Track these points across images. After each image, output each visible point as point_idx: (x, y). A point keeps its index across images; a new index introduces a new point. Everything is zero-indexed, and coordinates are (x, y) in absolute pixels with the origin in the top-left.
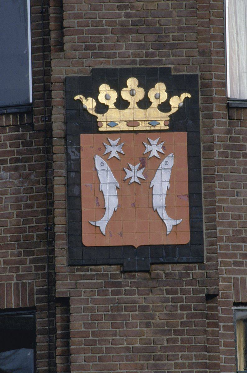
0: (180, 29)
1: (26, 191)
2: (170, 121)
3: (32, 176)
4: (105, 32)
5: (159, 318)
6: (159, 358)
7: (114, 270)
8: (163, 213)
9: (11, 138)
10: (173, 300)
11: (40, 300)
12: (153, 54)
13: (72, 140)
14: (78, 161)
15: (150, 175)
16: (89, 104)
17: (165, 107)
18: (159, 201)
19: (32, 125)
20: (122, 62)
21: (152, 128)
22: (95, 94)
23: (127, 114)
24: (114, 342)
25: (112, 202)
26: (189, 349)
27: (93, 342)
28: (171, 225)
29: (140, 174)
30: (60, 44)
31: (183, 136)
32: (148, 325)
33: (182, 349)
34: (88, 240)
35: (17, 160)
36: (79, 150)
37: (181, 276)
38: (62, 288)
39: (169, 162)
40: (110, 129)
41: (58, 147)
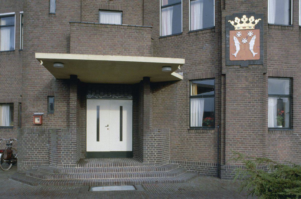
0: (258, 2)
1: (213, 48)
2: (255, 26)
4: (237, 4)
5: (250, 79)
6: (250, 90)
7: (238, 67)
8: (252, 51)
10: (254, 75)
11: (216, 76)
12: (250, 9)
13: (227, 33)
14: (229, 38)
15: (249, 41)
16: (232, 23)
17: (253, 23)
18: (251, 48)
19: (215, 31)
20: (241, 12)
21: (250, 29)
22: (234, 20)
23: (243, 25)
24: (238, 86)
25: (238, 48)
26: (258, 87)
27: (232, 86)
28: (255, 54)
29: (246, 41)
30: (224, 8)
31: (258, 30)
32: (247, 81)
33: (256, 87)
34: (231, 59)
35: (211, 41)
36: (229, 35)
37: (256, 68)
38: (224, 72)
39: (255, 37)
41: (223, 35)
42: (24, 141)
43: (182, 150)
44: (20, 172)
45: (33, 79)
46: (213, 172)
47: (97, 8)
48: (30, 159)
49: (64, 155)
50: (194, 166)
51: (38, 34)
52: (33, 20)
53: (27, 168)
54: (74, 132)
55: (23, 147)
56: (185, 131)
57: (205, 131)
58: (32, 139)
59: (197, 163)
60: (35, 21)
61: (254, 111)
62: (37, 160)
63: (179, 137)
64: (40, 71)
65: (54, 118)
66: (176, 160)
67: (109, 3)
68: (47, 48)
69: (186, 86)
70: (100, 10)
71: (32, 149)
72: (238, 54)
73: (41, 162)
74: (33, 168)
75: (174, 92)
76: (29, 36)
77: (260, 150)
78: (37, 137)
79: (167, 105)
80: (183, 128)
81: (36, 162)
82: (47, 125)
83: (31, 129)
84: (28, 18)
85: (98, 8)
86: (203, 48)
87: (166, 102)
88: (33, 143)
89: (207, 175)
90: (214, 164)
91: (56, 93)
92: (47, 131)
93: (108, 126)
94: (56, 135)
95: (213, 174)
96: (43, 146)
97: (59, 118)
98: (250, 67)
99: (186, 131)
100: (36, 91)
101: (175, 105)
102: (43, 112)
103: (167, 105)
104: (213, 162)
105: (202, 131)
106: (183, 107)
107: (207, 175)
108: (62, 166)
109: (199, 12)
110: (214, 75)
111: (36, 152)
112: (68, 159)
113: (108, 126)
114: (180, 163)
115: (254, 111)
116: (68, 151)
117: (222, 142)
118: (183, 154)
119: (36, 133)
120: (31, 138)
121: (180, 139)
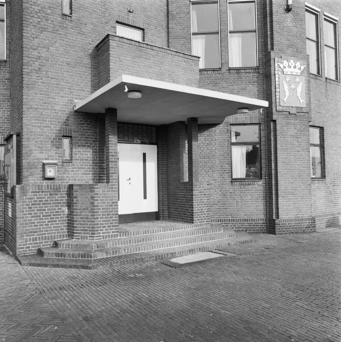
3: (259, 87)
9: (252, 76)
11: (262, 121)
18: (299, 95)
25: (287, 94)
40: (286, 73)
42: (27, 205)
43: (224, 206)
44: (22, 254)
45: (40, 109)
46: (262, 228)
47: (113, 18)
48: (37, 232)
49: (103, 221)
50: (239, 223)
51: (47, 41)
52: (39, 20)
53: (32, 247)
54: (115, 188)
55: (26, 214)
56: (228, 183)
57: (251, 182)
58: (40, 201)
59: (243, 219)
60: (42, 21)
61: (302, 160)
62: (48, 234)
63: (221, 191)
64: (51, 98)
65: (73, 168)
66: (218, 218)
67: (128, 16)
68: (61, 65)
69: (228, 130)
70: (117, 22)
71: (40, 216)
72: (287, 99)
73: (55, 236)
74: (43, 245)
75: (212, 137)
76: (33, 42)
77: (309, 201)
78: (48, 198)
79: (204, 153)
80: (225, 180)
81: (47, 235)
82: (62, 180)
83: (39, 185)
84: (31, 15)
85: (115, 18)
86: (246, 89)
87: (202, 149)
88: (42, 207)
89: (255, 232)
90: (263, 219)
91: (74, 132)
92: (62, 189)
93: (130, 179)
94: (90, 193)
95: (262, 230)
96: (57, 210)
97: (79, 168)
98: (298, 114)
99: (229, 184)
100: (45, 127)
101: (214, 153)
102: (56, 159)
103: (204, 153)
104: (262, 217)
105: (248, 183)
106: (224, 155)
107: (255, 232)
108: (100, 238)
109: (194, 45)
110: (259, 120)
111: (47, 220)
112: (108, 227)
113: (130, 179)
114: (223, 222)
115: (302, 160)
116: (108, 215)
117: (273, 194)
118: (226, 211)
119: (46, 192)
120: (38, 200)
121: (222, 193)
